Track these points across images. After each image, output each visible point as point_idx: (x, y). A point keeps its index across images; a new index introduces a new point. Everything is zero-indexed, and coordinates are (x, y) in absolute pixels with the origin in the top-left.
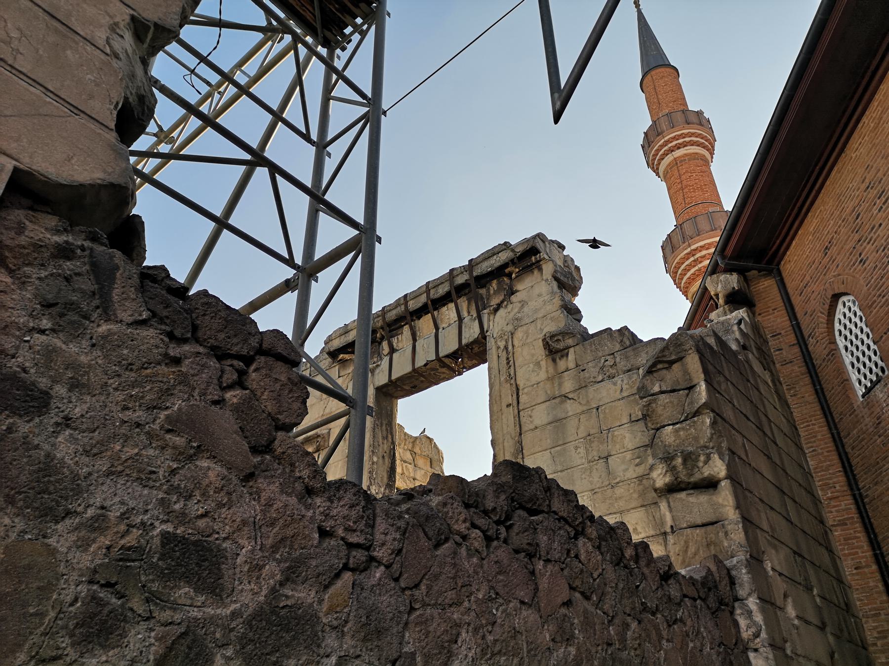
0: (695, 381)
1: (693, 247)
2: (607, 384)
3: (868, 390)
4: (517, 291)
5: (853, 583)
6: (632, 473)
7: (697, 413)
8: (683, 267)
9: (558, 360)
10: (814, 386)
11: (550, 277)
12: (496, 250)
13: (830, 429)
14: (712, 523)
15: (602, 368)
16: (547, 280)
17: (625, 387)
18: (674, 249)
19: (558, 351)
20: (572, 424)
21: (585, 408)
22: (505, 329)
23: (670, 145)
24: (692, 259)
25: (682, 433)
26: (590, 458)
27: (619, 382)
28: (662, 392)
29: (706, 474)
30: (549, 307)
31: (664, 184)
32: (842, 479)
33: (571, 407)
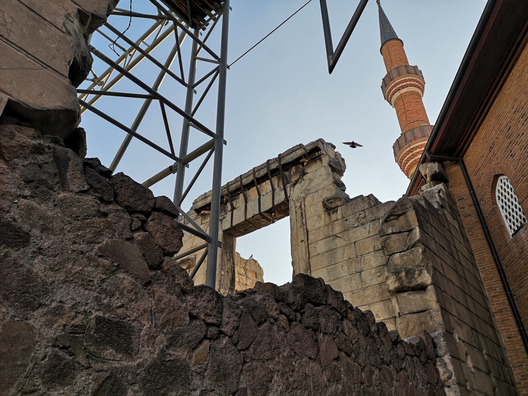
0: (413, 227)
1: (412, 147)
2: (361, 228)
3: (516, 232)
4: (307, 173)
5: (507, 347)
6: (375, 281)
7: (414, 246)
8: (406, 159)
9: (331, 214)
10: (484, 229)
11: (326, 165)
12: (295, 149)
13: (493, 255)
14: (423, 311)
15: (357, 219)
16: (325, 167)
17: (371, 230)
18: (400, 148)
19: (331, 209)
20: (339, 252)
21: (347, 243)
22: (300, 195)
23: (398, 86)
24: (411, 154)
25: (405, 257)
26: (350, 272)
27: (368, 227)
28: (393, 233)
29: (419, 282)
30: (326, 183)
31: (394, 109)
32: (500, 285)
33: (339, 242)
